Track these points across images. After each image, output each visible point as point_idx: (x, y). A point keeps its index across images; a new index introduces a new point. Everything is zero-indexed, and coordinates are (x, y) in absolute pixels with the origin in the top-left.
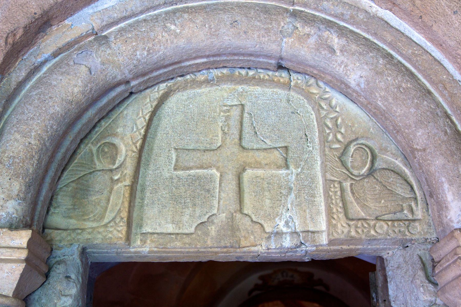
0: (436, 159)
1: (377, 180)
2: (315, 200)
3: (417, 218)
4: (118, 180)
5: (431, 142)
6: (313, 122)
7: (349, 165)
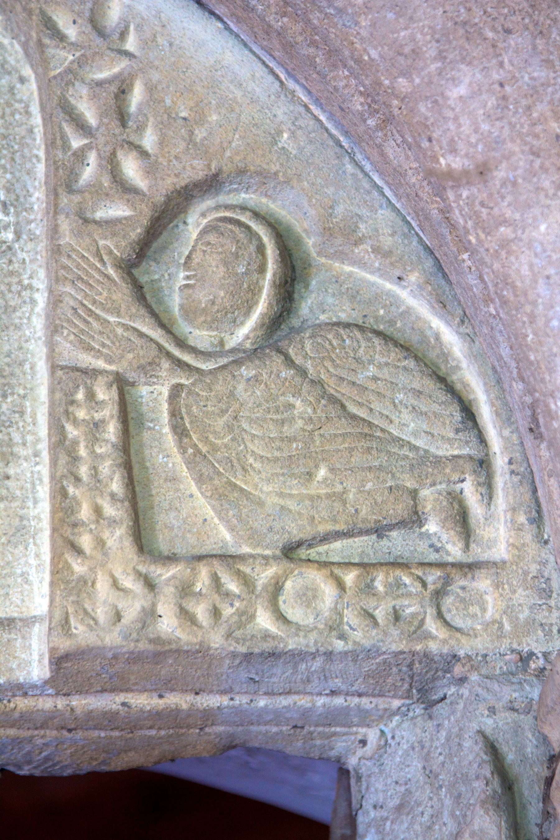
0: (536, 211)
1: (302, 372)
2: (11, 472)
3: (485, 556)
5: (512, 126)
6: (28, 113)
7: (175, 302)
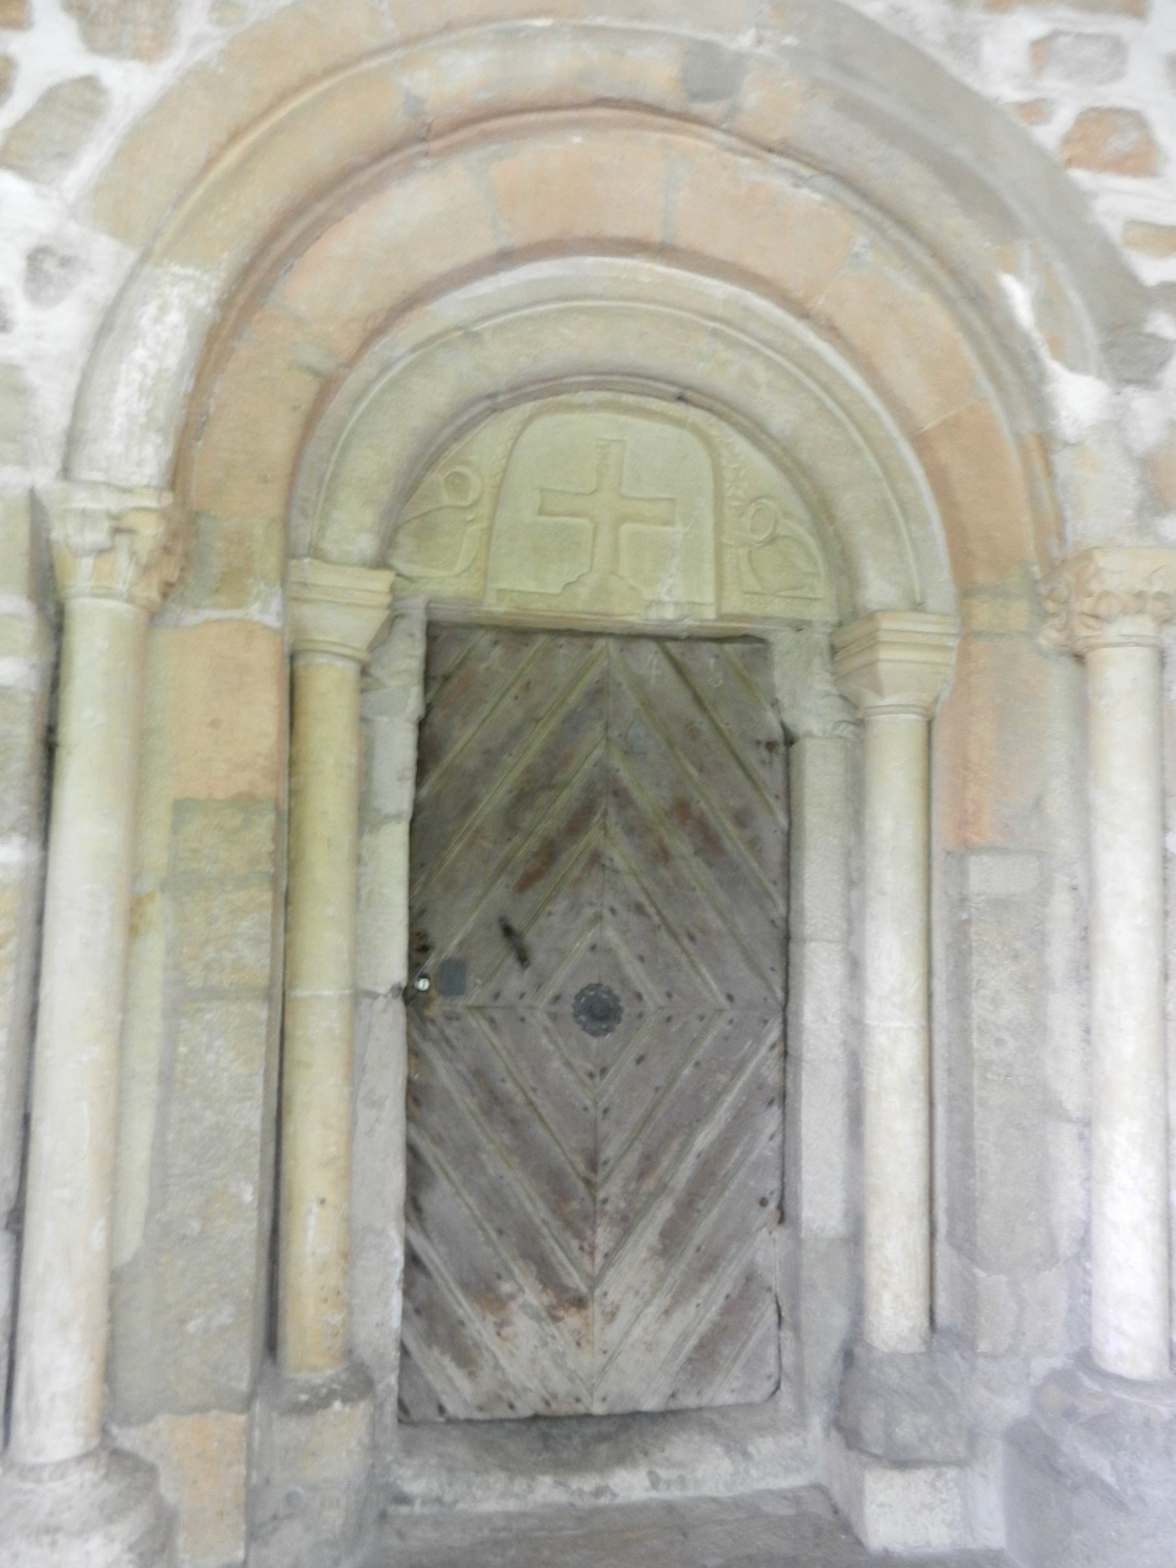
4: (471, 521)
